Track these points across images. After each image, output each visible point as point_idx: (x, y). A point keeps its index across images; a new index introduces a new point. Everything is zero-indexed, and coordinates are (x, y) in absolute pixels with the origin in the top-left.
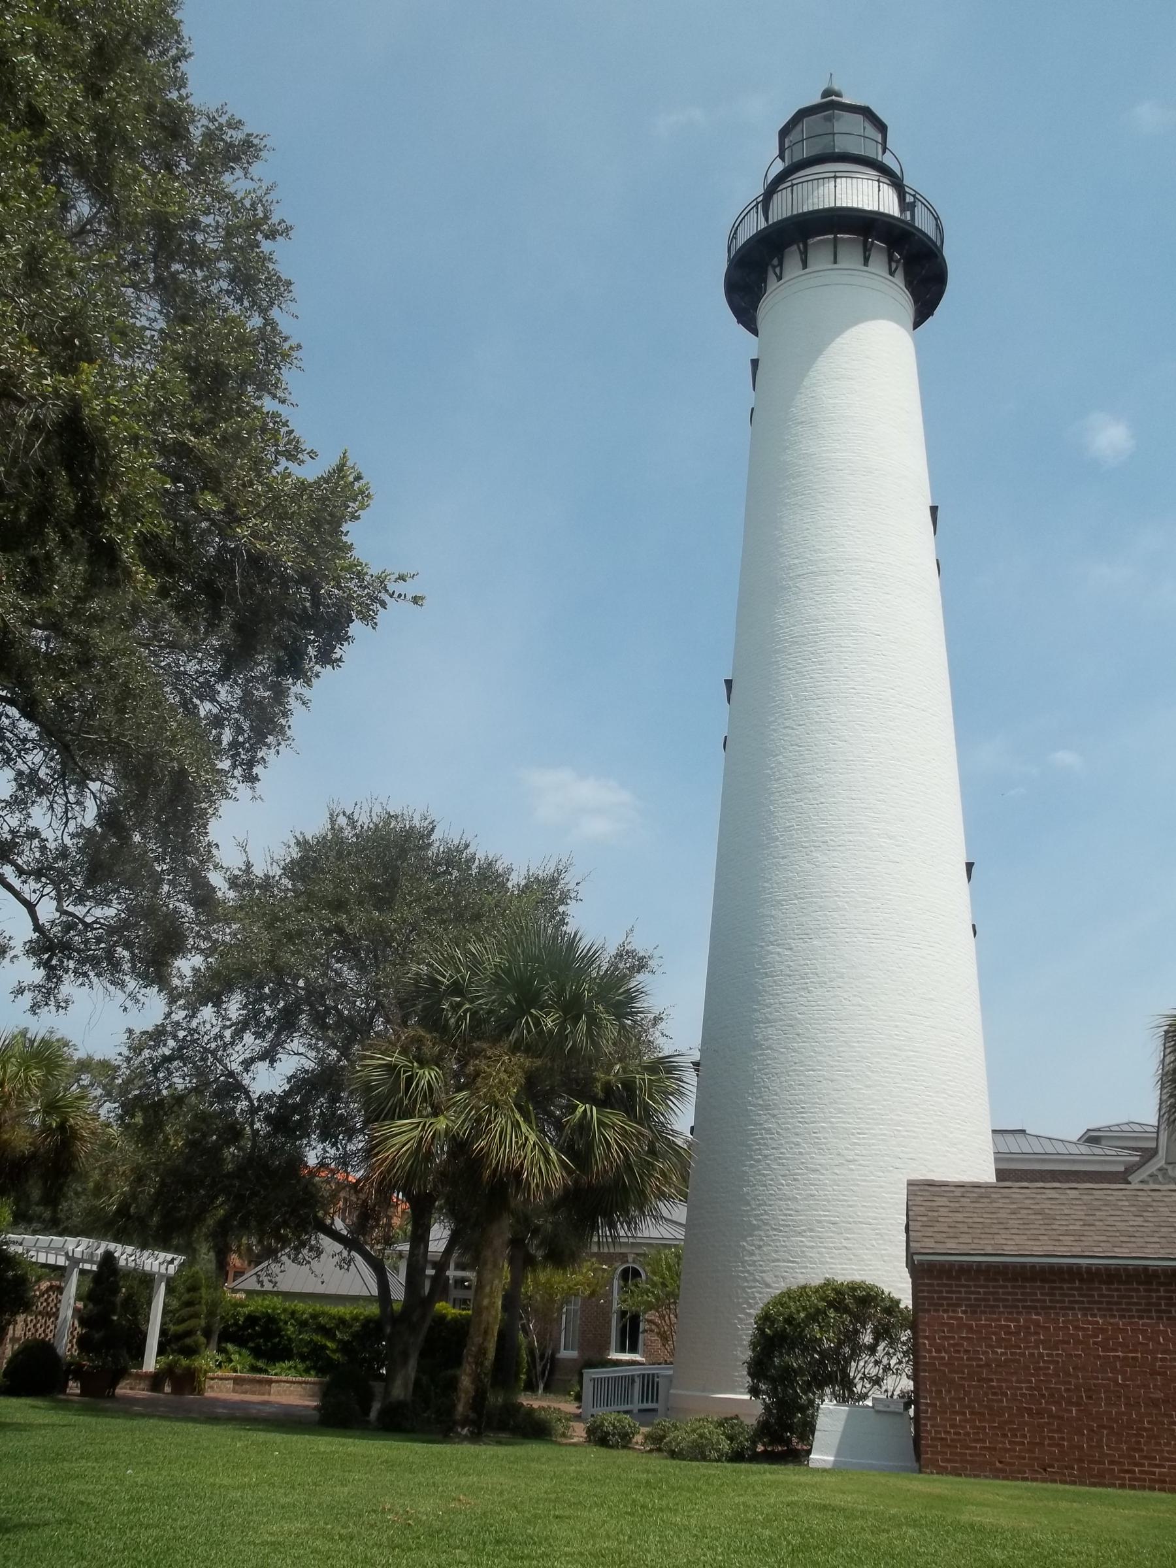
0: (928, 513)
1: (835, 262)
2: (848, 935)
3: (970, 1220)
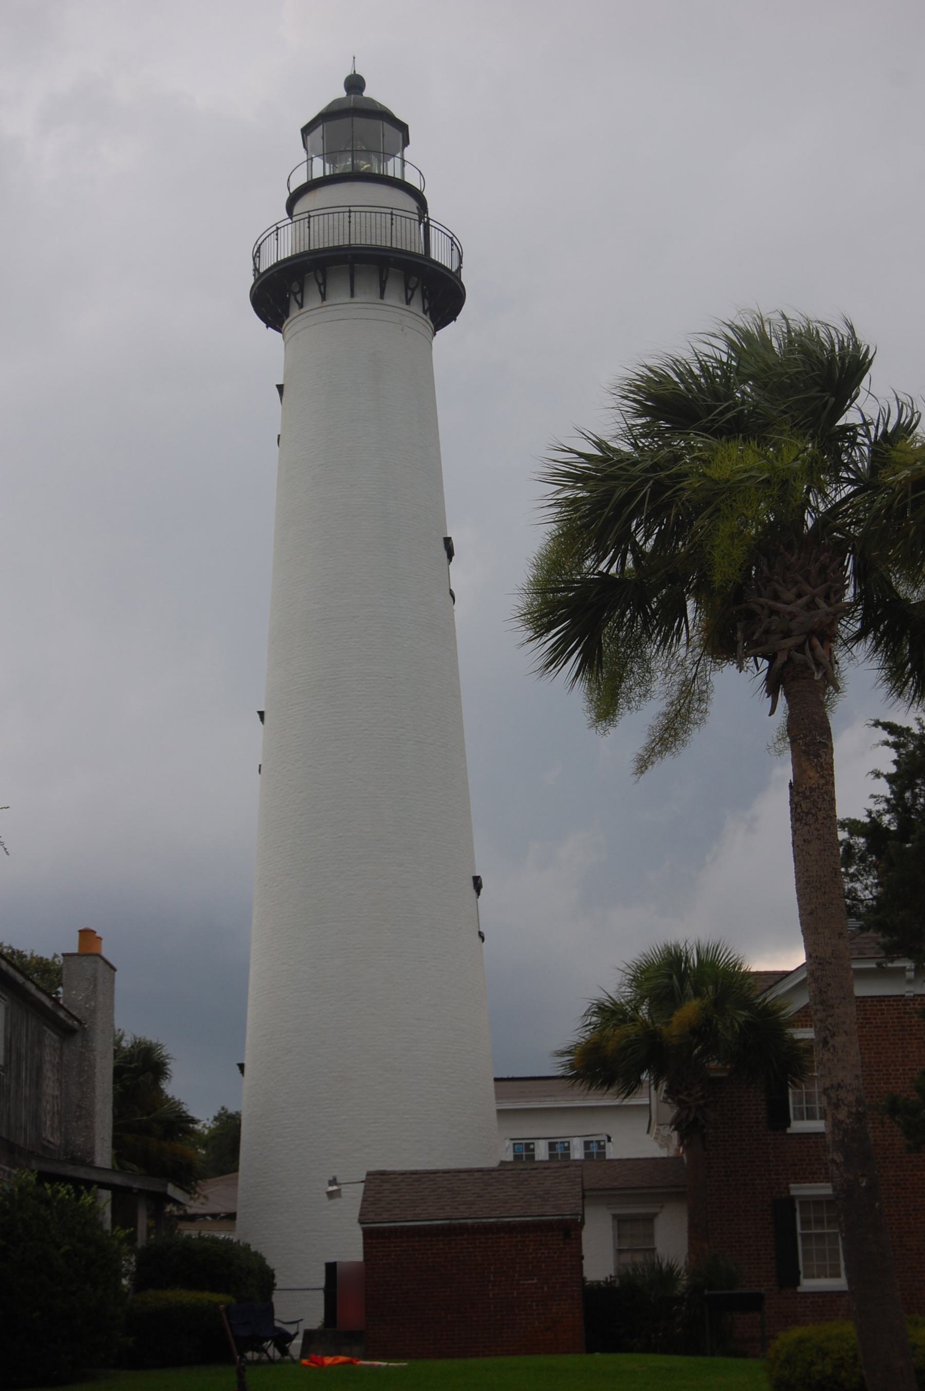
1: (352, 296)
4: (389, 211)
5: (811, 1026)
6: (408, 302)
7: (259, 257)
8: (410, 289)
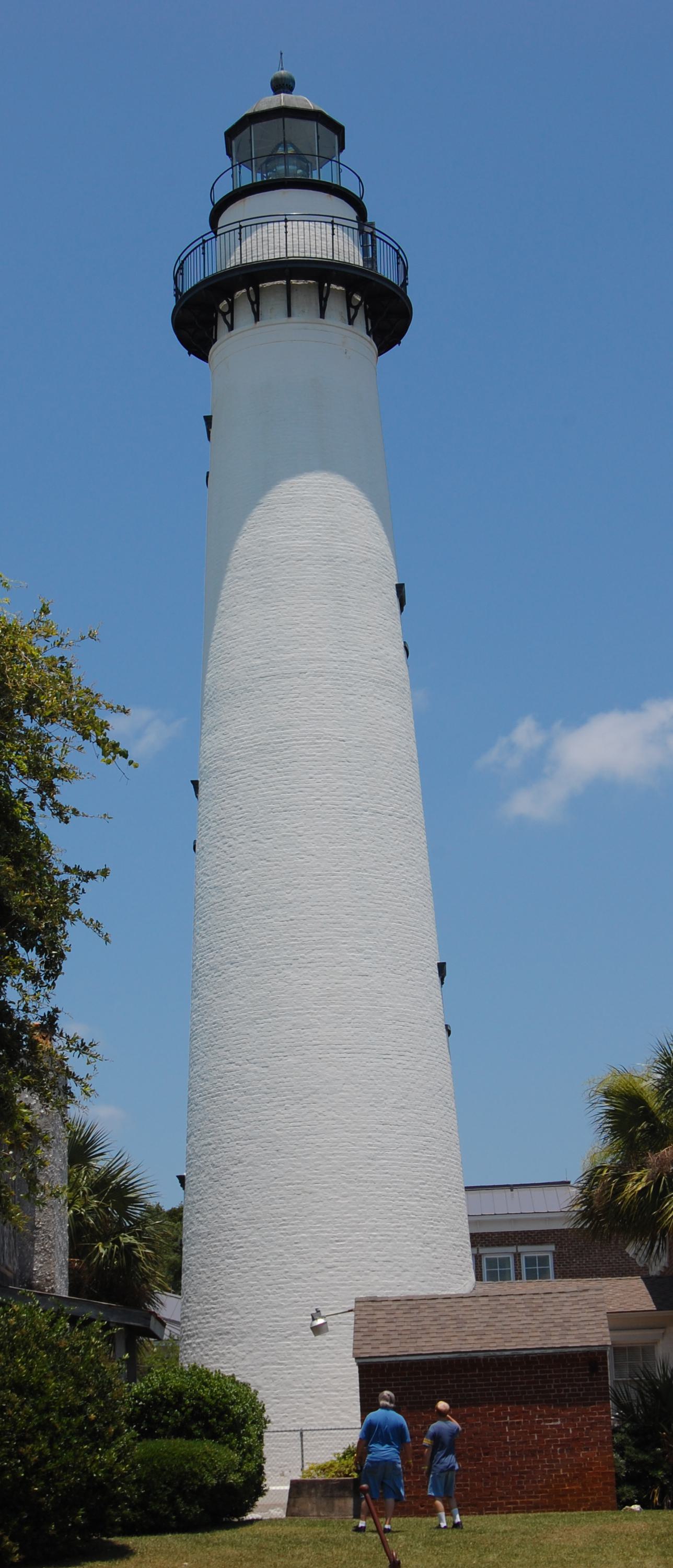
0: (394, 592)
2: (321, 1051)
3: (401, 1328)
4: (330, 219)
5: (552, 1243)
6: (351, 322)
7: (182, 274)
8: (353, 307)
